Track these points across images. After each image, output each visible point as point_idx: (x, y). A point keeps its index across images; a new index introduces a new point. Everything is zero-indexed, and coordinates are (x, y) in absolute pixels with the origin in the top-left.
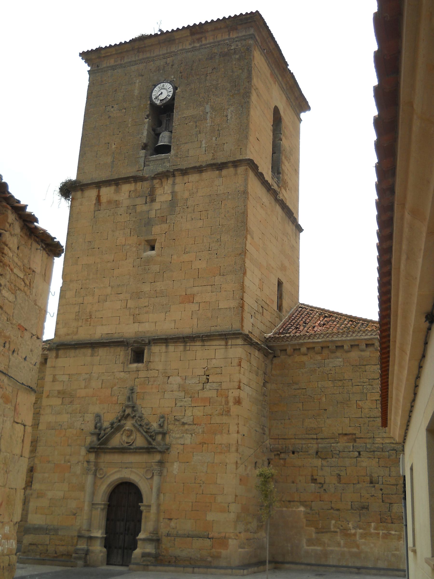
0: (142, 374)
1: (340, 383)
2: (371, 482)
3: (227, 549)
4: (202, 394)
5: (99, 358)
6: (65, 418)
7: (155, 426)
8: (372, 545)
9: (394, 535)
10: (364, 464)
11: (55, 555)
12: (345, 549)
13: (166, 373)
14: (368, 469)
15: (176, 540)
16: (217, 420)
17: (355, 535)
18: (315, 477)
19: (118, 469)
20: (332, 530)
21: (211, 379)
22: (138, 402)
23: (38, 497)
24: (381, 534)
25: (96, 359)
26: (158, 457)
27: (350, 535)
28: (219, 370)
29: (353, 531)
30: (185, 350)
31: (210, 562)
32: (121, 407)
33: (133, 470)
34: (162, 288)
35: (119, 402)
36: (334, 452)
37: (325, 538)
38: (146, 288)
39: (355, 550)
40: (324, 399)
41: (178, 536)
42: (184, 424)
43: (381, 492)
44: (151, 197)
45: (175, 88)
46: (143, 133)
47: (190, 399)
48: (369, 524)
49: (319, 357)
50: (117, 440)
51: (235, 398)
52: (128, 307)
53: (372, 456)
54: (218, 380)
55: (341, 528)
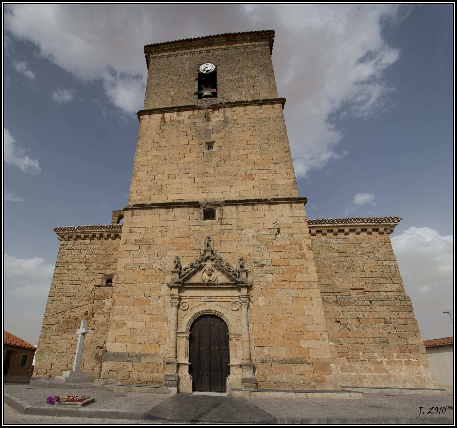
0: (216, 227)
1: (344, 255)
2: (386, 323)
3: (331, 374)
4: (275, 243)
5: (173, 215)
6: (143, 261)
7: (235, 267)
8: (398, 370)
9: (414, 362)
10: (377, 310)
11: (139, 382)
12: (376, 374)
13: (239, 226)
14: (381, 313)
15: (273, 366)
16: (295, 262)
17: (381, 362)
18: (338, 320)
19: (198, 302)
20: (362, 359)
21: (282, 231)
22: (215, 249)
23: (117, 327)
24: (403, 361)
25: (171, 217)
26: (244, 291)
27: (378, 363)
28: (288, 225)
29: (379, 360)
30: (253, 210)
31: (315, 387)
32: (199, 252)
33: (217, 303)
34: (225, 170)
35: (196, 248)
36: (351, 301)
37: (357, 365)
38: (211, 170)
39: (384, 374)
40: (333, 265)
41: (274, 361)
42: (263, 265)
43: (395, 330)
44: (208, 119)
45: (216, 66)
46: (195, 87)
47: (266, 246)
48: (391, 353)
49: (324, 237)
50: (196, 279)
51: (308, 246)
52: (195, 182)
53: (382, 304)
54: (289, 232)
55: (369, 358)
